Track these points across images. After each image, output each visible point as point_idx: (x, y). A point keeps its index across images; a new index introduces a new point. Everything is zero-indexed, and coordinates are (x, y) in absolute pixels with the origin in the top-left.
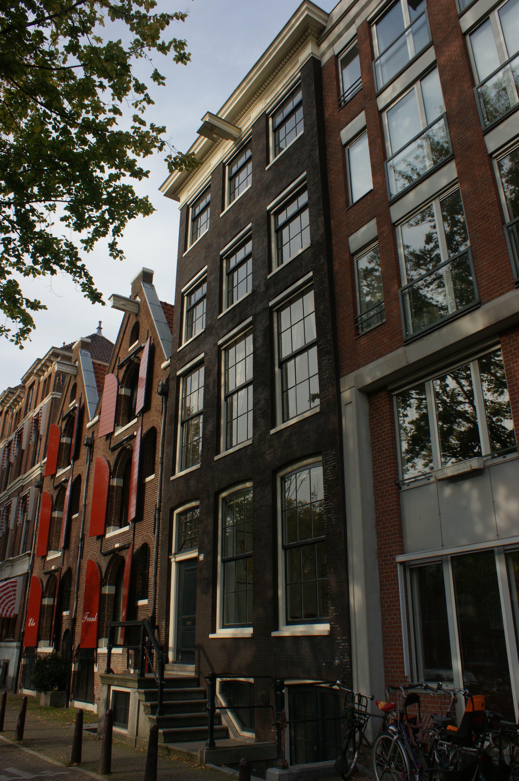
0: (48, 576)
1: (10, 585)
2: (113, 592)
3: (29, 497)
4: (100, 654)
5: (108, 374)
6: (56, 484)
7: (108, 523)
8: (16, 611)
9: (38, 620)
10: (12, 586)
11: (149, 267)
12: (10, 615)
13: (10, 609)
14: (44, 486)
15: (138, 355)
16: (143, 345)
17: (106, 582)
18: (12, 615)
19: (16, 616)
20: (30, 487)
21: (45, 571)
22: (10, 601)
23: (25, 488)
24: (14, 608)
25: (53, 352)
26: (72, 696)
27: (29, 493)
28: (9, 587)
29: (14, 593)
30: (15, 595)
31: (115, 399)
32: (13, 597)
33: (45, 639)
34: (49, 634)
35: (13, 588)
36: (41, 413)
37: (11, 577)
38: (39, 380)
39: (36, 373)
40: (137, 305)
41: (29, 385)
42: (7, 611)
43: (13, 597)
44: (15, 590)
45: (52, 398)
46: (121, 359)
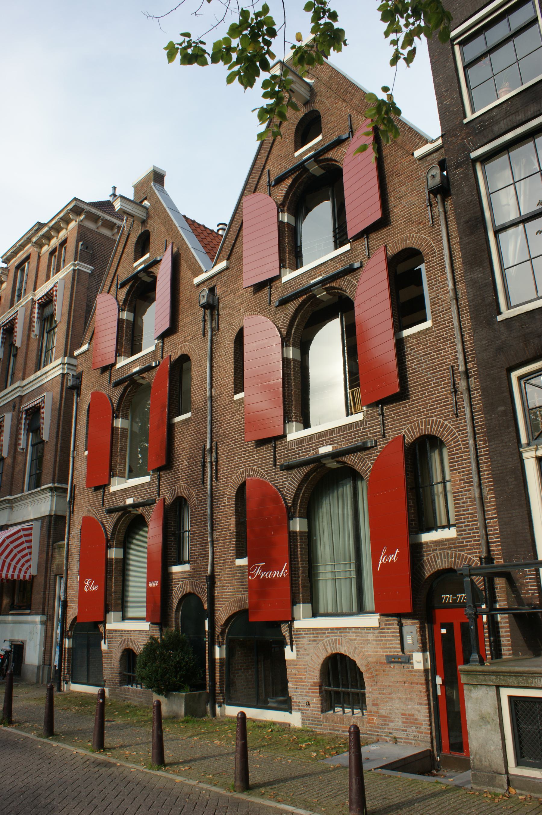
0: (116, 515)
1: (22, 533)
2: (121, 556)
3: (43, 408)
4: (298, 630)
5: (101, 293)
6: (114, 379)
7: (112, 473)
8: (33, 571)
9: (103, 583)
10: (25, 535)
11: (162, 167)
12: (24, 576)
13: (24, 569)
14: (83, 386)
15: (152, 270)
16: (159, 259)
17: (295, 512)
18: (27, 578)
19: (32, 578)
20: (45, 394)
21: (107, 506)
22: (23, 557)
23: (25, 399)
24: (30, 566)
25: (75, 206)
26: (220, 698)
27: (43, 401)
28: (21, 537)
29: (28, 544)
30: (30, 547)
31: (116, 323)
32: (27, 551)
33: (115, 611)
34: (120, 602)
35: (28, 538)
36: (56, 291)
37: (10, 523)
38: (39, 253)
39: (35, 243)
40: (145, 210)
41: (16, 264)
42: (20, 570)
43: (27, 551)
44: (30, 541)
45: (74, 270)
46: (272, 173)
